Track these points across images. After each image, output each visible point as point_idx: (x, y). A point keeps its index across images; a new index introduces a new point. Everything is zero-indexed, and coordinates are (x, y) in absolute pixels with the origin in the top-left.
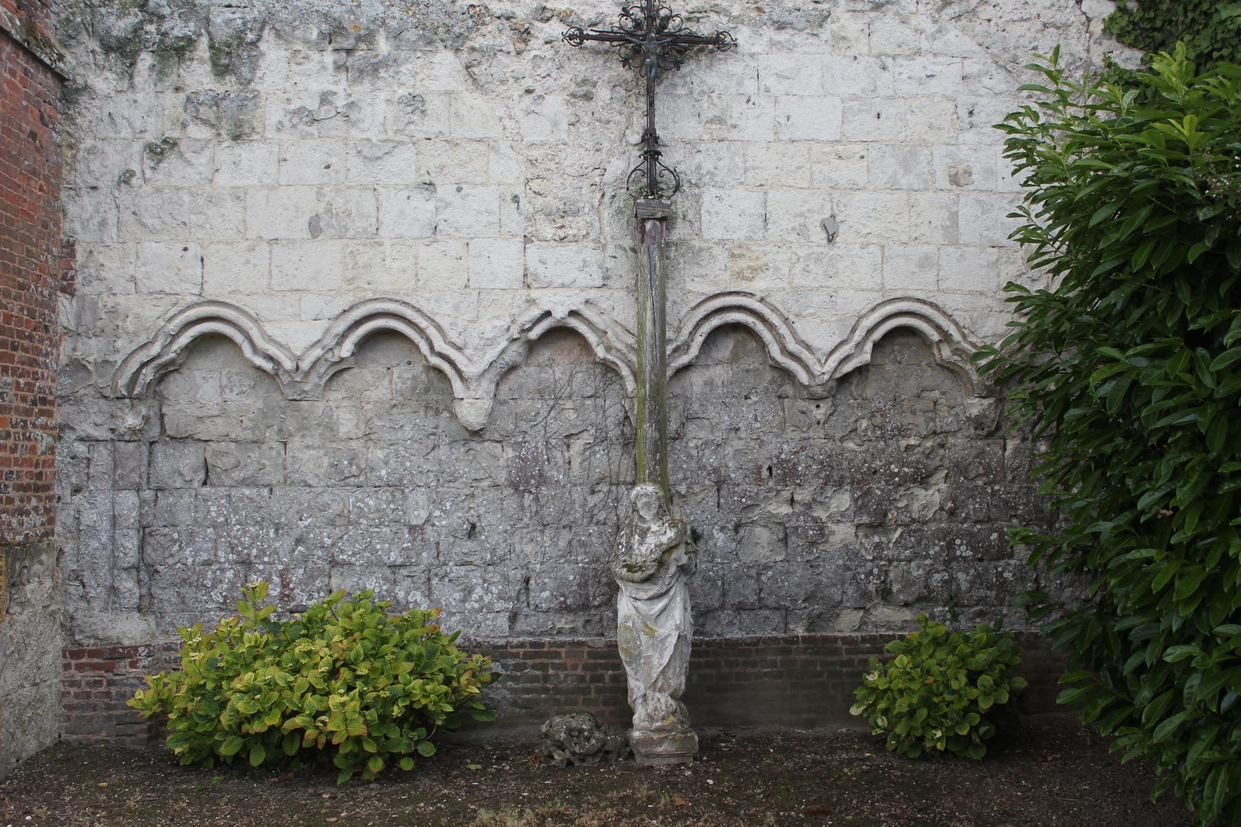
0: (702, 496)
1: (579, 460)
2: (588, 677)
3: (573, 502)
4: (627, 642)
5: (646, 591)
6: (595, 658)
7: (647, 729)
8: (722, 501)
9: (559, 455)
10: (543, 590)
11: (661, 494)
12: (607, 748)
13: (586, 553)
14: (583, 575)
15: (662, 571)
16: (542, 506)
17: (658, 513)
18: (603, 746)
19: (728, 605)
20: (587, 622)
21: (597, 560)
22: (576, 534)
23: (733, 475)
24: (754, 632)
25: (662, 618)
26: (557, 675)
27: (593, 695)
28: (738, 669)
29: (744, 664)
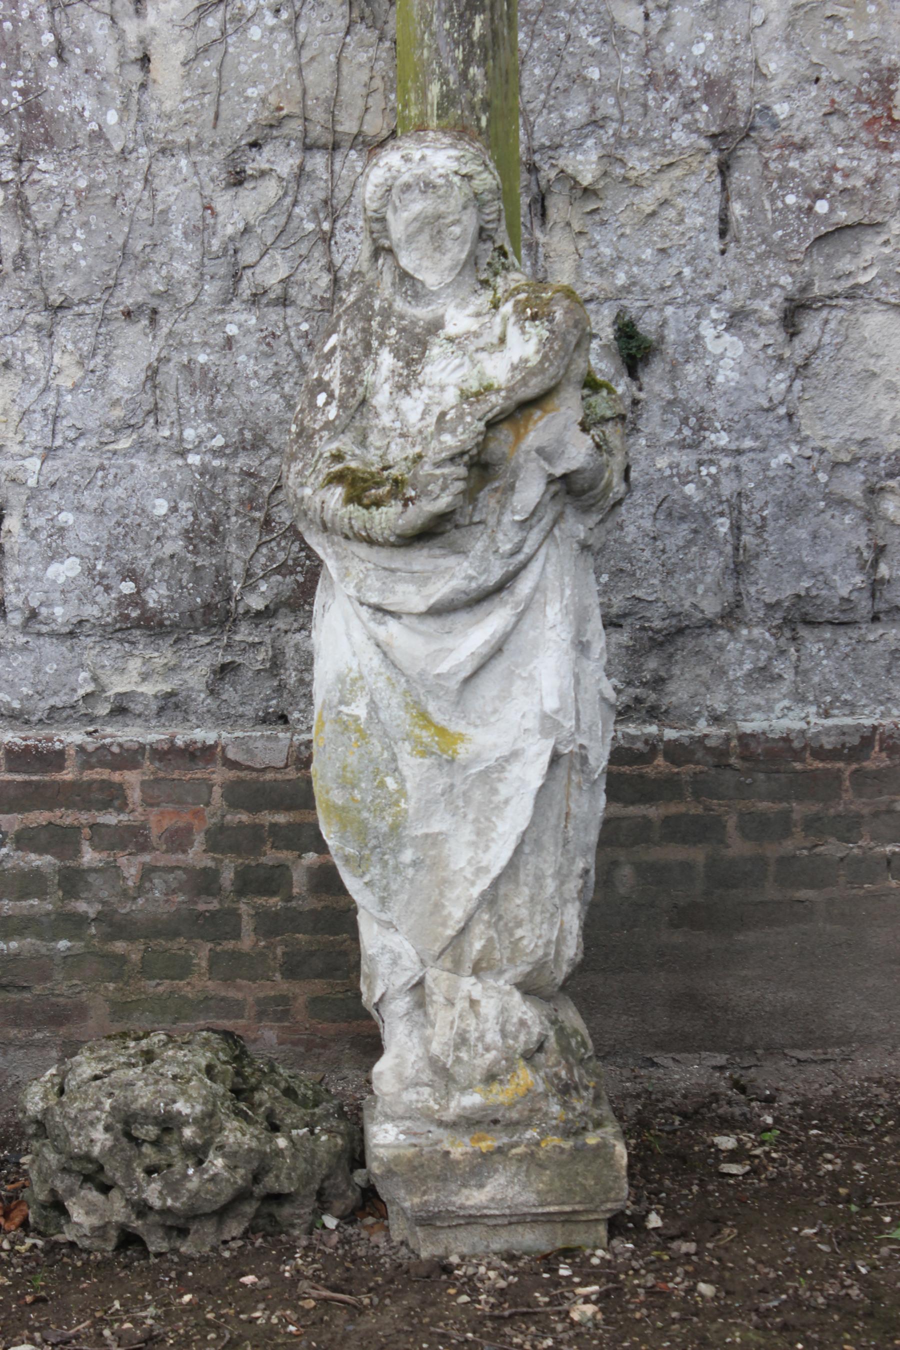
0: (660, 189)
1: (181, 50)
2: (228, 877)
3: (163, 218)
4: (347, 783)
5: (422, 579)
6: (253, 809)
7: (427, 1115)
8: (737, 209)
9: (100, 29)
10: (54, 555)
11: (487, 180)
12: (270, 1183)
13: (214, 414)
14: (203, 498)
15: (488, 499)
16: (41, 235)
17: (473, 260)
18: (256, 1178)
19: (753, 610)
20: (224, 671)
21: (258, 442)
22: (177, 343)
23: (782, 109)
24: (851, 708)
25: (489, 685)
26: (112, 870)
27: (247, 942)
28: (788, 846)
29: (813, 825)
